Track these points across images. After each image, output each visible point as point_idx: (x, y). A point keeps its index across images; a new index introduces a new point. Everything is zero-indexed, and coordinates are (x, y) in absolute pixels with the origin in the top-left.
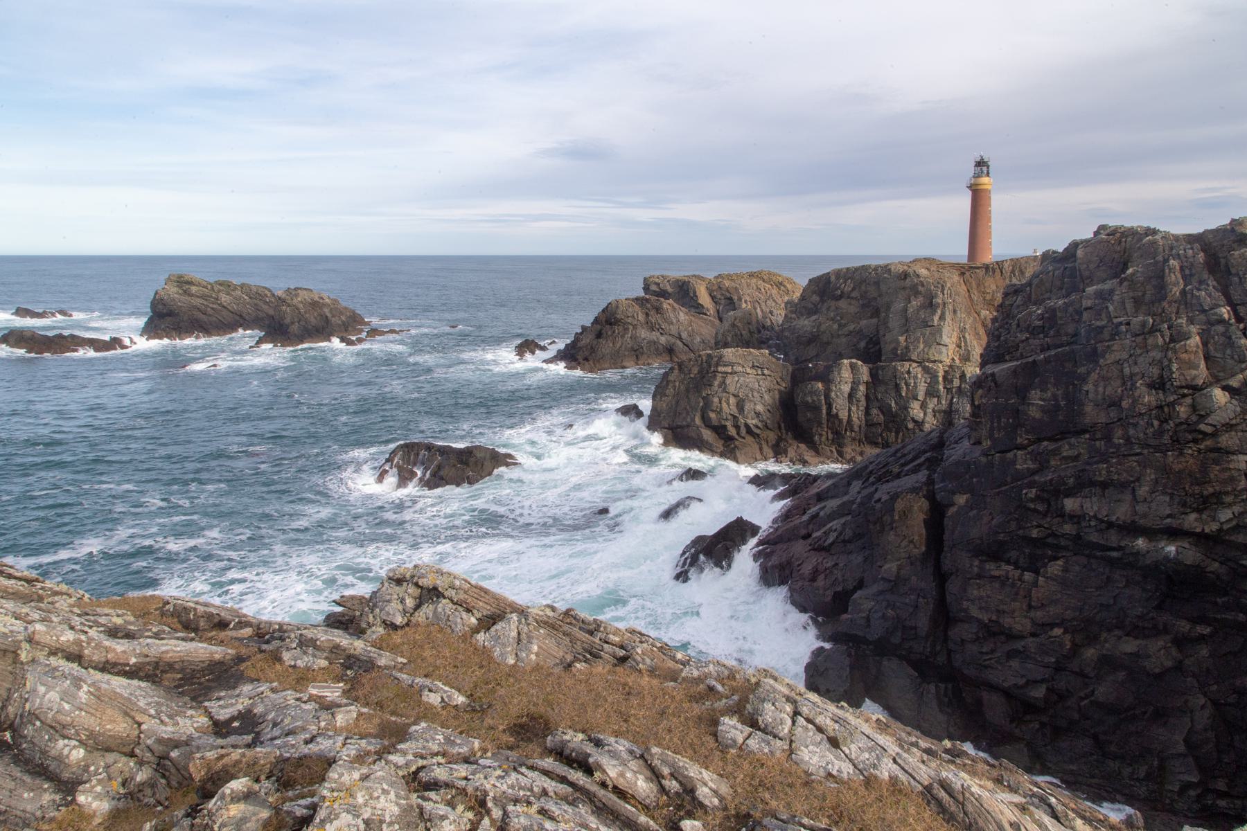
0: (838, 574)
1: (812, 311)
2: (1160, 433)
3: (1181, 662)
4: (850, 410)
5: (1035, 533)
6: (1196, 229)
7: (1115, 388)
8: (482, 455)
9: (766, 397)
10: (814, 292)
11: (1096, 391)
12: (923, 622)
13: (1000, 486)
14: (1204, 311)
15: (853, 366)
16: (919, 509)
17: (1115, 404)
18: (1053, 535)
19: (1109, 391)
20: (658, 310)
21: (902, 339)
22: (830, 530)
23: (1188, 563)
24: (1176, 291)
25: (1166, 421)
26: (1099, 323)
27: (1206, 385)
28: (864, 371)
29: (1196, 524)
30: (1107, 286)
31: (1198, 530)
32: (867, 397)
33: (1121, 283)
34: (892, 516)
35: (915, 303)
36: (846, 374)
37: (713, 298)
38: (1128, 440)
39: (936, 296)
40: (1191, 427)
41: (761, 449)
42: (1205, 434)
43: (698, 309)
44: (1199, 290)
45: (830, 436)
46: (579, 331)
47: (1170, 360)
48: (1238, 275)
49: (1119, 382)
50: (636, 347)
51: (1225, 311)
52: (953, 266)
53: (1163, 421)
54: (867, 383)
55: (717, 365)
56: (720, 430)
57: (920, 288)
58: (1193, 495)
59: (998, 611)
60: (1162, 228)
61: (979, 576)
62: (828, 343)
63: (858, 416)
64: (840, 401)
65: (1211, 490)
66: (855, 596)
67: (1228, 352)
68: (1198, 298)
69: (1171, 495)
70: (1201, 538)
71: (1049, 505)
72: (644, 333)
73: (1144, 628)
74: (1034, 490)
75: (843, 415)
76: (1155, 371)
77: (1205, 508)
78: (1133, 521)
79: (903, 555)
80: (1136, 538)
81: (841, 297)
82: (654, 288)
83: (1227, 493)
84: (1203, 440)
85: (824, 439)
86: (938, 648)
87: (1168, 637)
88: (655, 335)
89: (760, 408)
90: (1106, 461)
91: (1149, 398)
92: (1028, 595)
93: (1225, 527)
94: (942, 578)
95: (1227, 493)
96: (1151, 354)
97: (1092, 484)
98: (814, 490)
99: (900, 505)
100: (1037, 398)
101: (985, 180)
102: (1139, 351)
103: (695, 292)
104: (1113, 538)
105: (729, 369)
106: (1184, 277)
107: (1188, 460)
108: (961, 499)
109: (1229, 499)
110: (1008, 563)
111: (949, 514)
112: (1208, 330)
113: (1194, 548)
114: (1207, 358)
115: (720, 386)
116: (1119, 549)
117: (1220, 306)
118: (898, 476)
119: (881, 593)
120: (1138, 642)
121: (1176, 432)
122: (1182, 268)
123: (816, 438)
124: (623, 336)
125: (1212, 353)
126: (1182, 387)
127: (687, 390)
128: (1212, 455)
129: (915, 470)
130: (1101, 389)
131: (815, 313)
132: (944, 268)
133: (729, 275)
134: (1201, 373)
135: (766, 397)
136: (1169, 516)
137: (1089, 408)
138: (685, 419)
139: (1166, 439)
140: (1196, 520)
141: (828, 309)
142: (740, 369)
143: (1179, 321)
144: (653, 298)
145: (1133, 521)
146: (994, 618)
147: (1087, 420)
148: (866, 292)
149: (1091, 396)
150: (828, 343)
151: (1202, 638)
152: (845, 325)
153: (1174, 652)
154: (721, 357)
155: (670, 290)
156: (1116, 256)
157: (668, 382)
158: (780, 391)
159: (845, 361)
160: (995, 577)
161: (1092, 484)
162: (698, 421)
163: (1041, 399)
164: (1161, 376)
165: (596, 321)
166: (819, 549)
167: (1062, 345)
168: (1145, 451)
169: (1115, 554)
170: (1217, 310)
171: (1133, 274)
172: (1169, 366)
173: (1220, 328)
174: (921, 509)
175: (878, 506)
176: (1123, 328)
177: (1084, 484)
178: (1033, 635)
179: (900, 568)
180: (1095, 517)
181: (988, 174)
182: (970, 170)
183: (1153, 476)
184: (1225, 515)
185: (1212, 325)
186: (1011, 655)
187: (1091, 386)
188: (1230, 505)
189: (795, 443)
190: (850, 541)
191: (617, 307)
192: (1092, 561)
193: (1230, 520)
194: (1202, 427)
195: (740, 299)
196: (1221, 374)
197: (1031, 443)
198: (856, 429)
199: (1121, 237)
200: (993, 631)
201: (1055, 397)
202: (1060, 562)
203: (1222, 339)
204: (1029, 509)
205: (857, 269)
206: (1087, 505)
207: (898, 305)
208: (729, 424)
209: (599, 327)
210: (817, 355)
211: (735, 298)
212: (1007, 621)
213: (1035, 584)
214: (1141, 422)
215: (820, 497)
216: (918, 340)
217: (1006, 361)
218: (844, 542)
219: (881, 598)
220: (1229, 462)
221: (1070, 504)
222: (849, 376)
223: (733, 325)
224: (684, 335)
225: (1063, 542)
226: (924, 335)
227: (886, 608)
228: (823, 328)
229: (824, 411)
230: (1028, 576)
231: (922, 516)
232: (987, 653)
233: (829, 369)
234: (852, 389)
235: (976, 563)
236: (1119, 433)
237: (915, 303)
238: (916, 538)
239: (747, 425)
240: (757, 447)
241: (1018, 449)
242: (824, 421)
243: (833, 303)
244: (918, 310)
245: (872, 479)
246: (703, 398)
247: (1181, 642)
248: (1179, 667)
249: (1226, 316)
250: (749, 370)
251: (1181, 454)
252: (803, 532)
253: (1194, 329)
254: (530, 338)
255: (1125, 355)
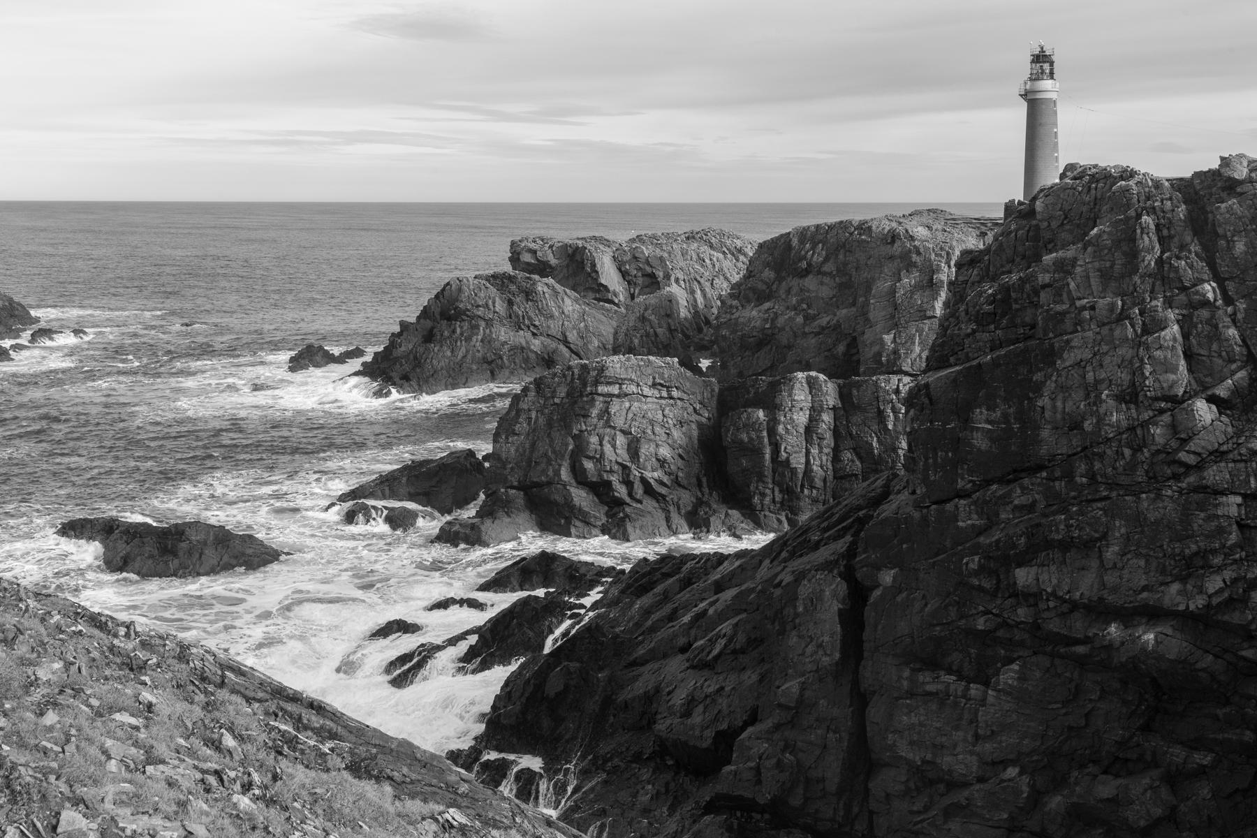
0: (723, 703)
1: (762, 297)
2: (1132, 467)
3: (1174, 809)
4: (808, 453)
5: (981, 624)
6: (1185, 171)
7: (1076, 403)
8: (201, 537)
9: (676, 434)
10: (768, 265)
11: (1054, 407)
12: (832, 770)
13: (937, 554)
14: (1184, 289)
15: (811, 383)
16: (832, 592)
17: (1075, 425)
18: (1005, 624)
19: (1069, 406)
20: (529, 294)
21: (888, 338)
22: (718, 636)
23: (1172, 657)
24: (1150, 260)
25: (1140, 449)
26: (1059, 308)
27: (1190, 395)
28: (830, 391)
29: (1179, 599)
30: (1070, 253)
31: (1182, 607)
32: (836, 433)
33: (1085, 248)
34: (795, 607)
35: (907, 281)
36: (801, 395)
37: (624, 274)
38: (1092, 477)
39: (939, 270)
40: (1167, 455)
41: (668, 519)
42: (1188, 467)
43: (600, 293)
44: (1178, 258)
45: (778, 497)
46: (397, 329)
47: (1142, 360)
48: (1225, 236)
49: (1081, 393)
50: (490, 356)
51: (1209, 290)
52: (968, 222)
53: (1137, 450)
54: (834, 408)
55: (597, 383)
56: (600, 489)
57: (914, 257)
58: (1173, 556)
59: (934, 746)
60: (1141, 166)
61: (911, 694)
62: (789, 347)
63: (820, 462)
64: (791, 439)
65: (1194, 547)
66: (744, 735)
67: (1215, 347)
68: (1177, 269)
69: (1147, 558)
70: (1187, 620)
71: (999, 581)
72: (503, 334)
73: (1127, 760)
74: (976, 558)
75: (798, 462)
76: (1125, 376)
77: (1189, 575)
78: (1101, 599)
79: (809, 667)
80: (1108, 624)
81: (806, 273)
82: (527, 258)
83: (1214, 552)
84: (1186, 474)
85: (767, 500)
86: (856, 810)
87: (1156, 773)
88: (522, 337)
89: (665, 452)
90: (1064, 510)
91: (1116, 417)
92: (973, 721)
93: (1215, 601)
94: (861, 700)
95: (1214, 552)
96: (1120, 352)
97: (1049, 545)
98: (716, 576)
99: (805, 589)
100: (982, 419)
101: (1046, 84)
102: (1105, 348)
103: (594, 265)
104: (1078, 625)
105: (615, 390)
106: (1161, 240)
107: (1162, 507)
108: (887, 577)
109: (1217, 560)
110: (950, 671)
111: (872, 600)
112: (1190, 316)
113: (1178, 635)
114: (1188, 355)
115: (600, 417)
116: (1086, 640)
117: (1203, 281)
118: (816, 546)
119: (777, 727)
120: (1120, 781)
121: (1152, 464)
122: (1158, 227)
123: (756, 500)
124: (468, 339)
125: (1196, 349)
126: (1156, 399)
127: (550, 424)
128: (1196, 497)
129: (836, 538)
130: (1059, 404)
131: (768, 298)
132: (954, 226)
133: (654, 237)
134: (1181, 377)
135: (676, 434)
136: (1145, 588)
137: (1045, 433)
138: (544, 472)
139: (1140, 476)
140: (1179, 593)
141: (788, 291)
142: (633, 388)
143: (1154, 303)
144: (520, 275)
145: (1101, 599)
146: (929, 757)
147: (1044, 451)
148: (845, 264)
149: (1047, 414)
150: (789, 347)
151: (1202, 771)
152: (814, 318)
153: (1164, 793)
154: (602, 369)
155: (553, 261)
156: (1085, 209)
157: (518, 412)
158: (700, 425)
159: (800, 375)
160: (930, 694)
161: (1049, 545)
162: (565, 474)
163: (988, 422)
164: (1132, 384)
165: (425, 313)
166: (703, 666)
167: (1017, 341)
168: (1114, 494)
169: (1081, 649)
170: (1199, 288)
171: (1099, 236)
172: (1141, 368)
173: (1204, 313)
174: (834, 595)
175: (778, 592)
176: (1086, 314)
177: (1037, 547)
178: (981, 780)
179: (803, 686)
180: (1054, 594)
181: (1051, 75)
182: (1026, 68)
183: (1123, 530)
184: (1214, 584)
185: (1195, 308)
186: (948, 813)
187: (1046, 400)
188: (1220, 569)
189: (723, 509)
190: (743, 651)
191: (460, 290)
192: (1057, 661)
193: (1221, 591)
194: (1182, 456)
195: (667, 276)
196: (1208, 379)
197: (978, 487)
198: (819, 483)
199: (1090, 182)
200: (928, 779)
201: (1005, 416)
202: (1015, 667)
203: (1207, 328)
204: (973, 587)
205: (831, 227)
206: (1044, 577)
207: (883, 285)
208: (614, 479)
209: (429, 323)
210: (772, 367)
211: (660, 274)
212: (946, 761)
213: (983, 702)
214: (1109, 452)
215: (719, 587)
216: (911, 339)
217: (951, 366)
218: (734, 654)
219: (776, 736)
220: (1216, 506)
221: (1023, 576)
222: (806, 398)
223: (643, 319)
224: (572, 336)
225: (1018, 635)
226: (920, 331)
227: (783, 751)
228: (781, 321)
229: (768, 456)
230: (975, 690)
231: (836, 606)
232: (919, 812)
233: (774, 388)
234: (811, 419)
235: (906, 673)
236: (1082, 467)
237: (907, 281)
238: (826, 639)
239: (644, 481)
240: (660, 516)
241: (960, 497)
242: (768, 472)
243: (794, 283)
244: (912, 293)
245: (784, 554)
246: (575, 437)
247: (1175, 779)
248: (1171, 817)
249: (1210, 296)
250: (647, 391)
251: (1159, 496)
252: (682, 641)
253: (1171, 315)
254: (312, 340)
255: (1087, 355)
